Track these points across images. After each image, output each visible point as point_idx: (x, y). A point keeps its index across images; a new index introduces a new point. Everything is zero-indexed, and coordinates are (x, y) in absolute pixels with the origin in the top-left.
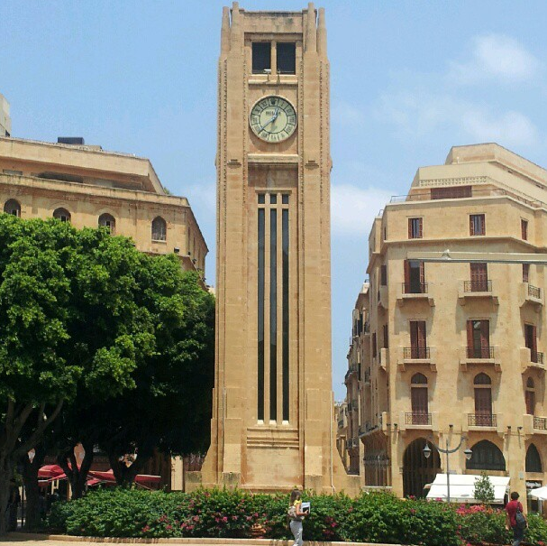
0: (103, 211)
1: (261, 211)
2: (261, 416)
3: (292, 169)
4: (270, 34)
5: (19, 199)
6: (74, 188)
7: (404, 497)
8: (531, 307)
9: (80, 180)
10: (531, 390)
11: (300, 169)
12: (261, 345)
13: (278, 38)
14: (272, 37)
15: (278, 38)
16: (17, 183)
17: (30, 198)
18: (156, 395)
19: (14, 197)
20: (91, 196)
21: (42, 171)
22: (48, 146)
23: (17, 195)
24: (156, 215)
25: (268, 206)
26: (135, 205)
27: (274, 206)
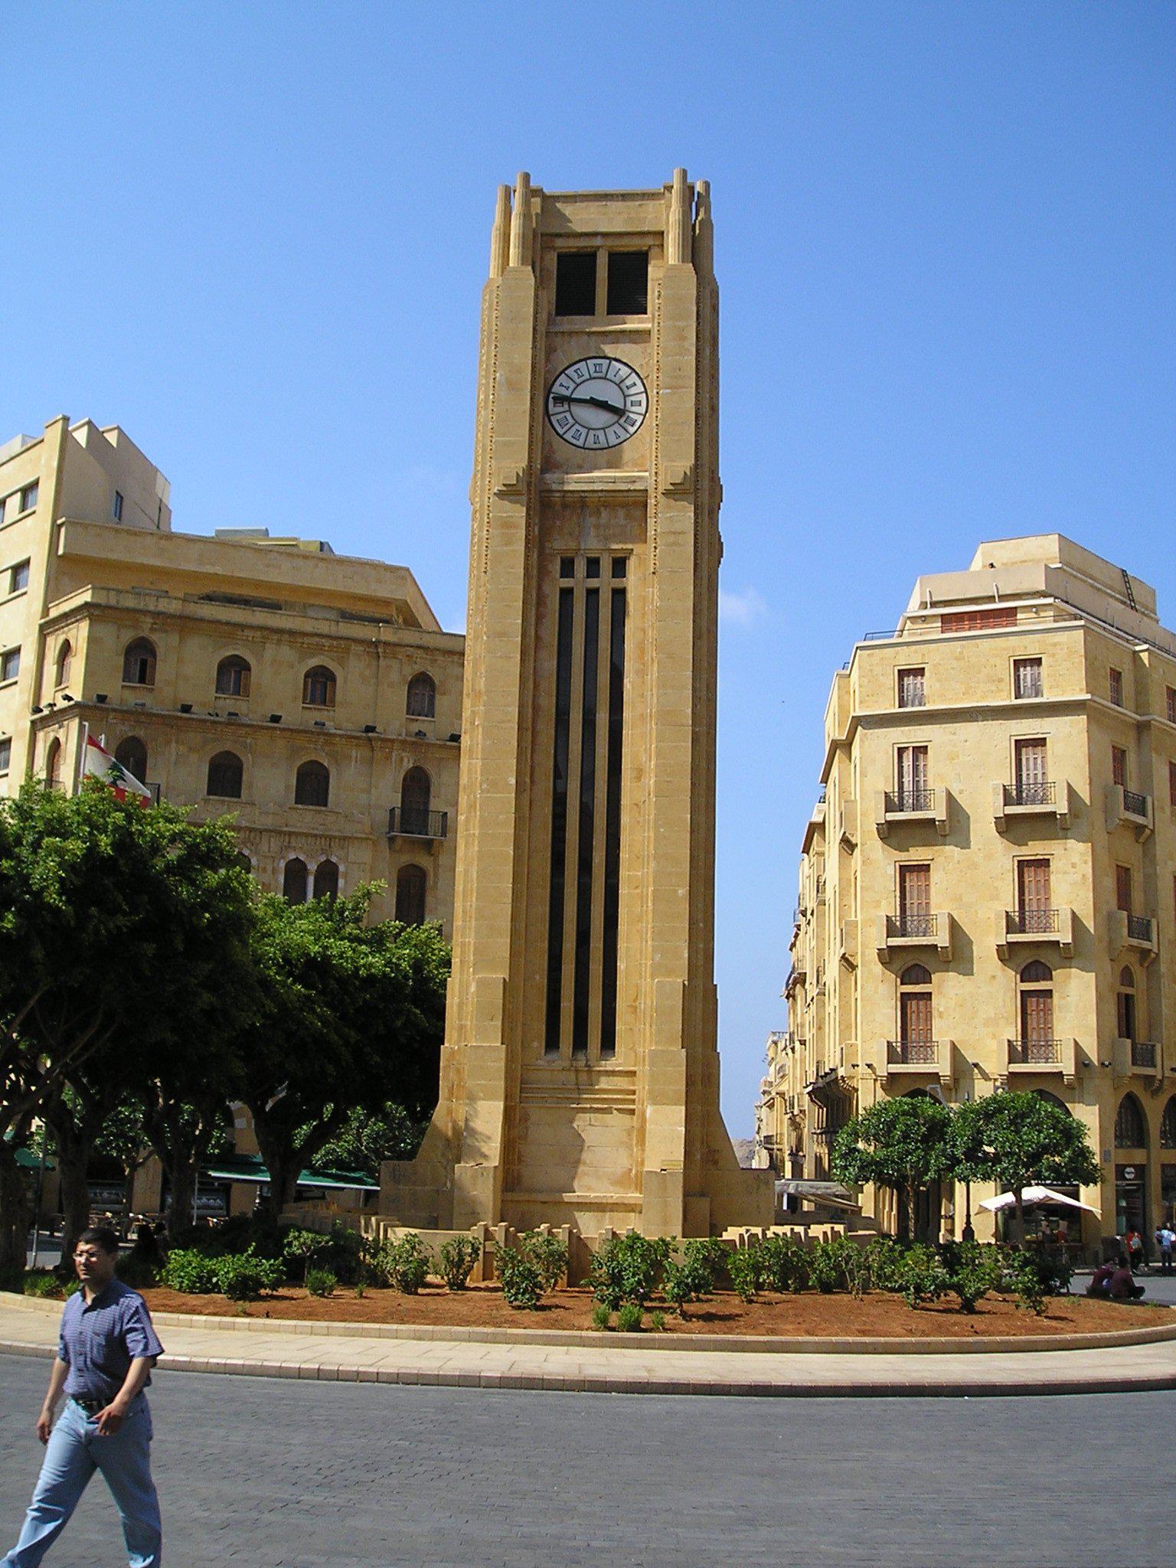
0: (313, 662)
1: (567, 594)
2: (552, 1042)
3: (635, 504)
4: (595, 234)
5: (154, 637)
6: (260, 617)
7: (851, 1293)
8: (825, 780)
9: (274, 606)
10: (1129, 991)
11: (651, 502)
12: (560, 801)
13: (610, 242)
14: (598, 241)
15: (610, 242)
16: (152, 608)
17: (174, 639)
18: (211, 1225)
19: (145, 633)
20: (291, 633)
21: (207, 590)
22: (232, 546)
23: (152, 630)
24: (418, 668)
25: (580, 582)
26: (375, 648)
27: (593, 583)
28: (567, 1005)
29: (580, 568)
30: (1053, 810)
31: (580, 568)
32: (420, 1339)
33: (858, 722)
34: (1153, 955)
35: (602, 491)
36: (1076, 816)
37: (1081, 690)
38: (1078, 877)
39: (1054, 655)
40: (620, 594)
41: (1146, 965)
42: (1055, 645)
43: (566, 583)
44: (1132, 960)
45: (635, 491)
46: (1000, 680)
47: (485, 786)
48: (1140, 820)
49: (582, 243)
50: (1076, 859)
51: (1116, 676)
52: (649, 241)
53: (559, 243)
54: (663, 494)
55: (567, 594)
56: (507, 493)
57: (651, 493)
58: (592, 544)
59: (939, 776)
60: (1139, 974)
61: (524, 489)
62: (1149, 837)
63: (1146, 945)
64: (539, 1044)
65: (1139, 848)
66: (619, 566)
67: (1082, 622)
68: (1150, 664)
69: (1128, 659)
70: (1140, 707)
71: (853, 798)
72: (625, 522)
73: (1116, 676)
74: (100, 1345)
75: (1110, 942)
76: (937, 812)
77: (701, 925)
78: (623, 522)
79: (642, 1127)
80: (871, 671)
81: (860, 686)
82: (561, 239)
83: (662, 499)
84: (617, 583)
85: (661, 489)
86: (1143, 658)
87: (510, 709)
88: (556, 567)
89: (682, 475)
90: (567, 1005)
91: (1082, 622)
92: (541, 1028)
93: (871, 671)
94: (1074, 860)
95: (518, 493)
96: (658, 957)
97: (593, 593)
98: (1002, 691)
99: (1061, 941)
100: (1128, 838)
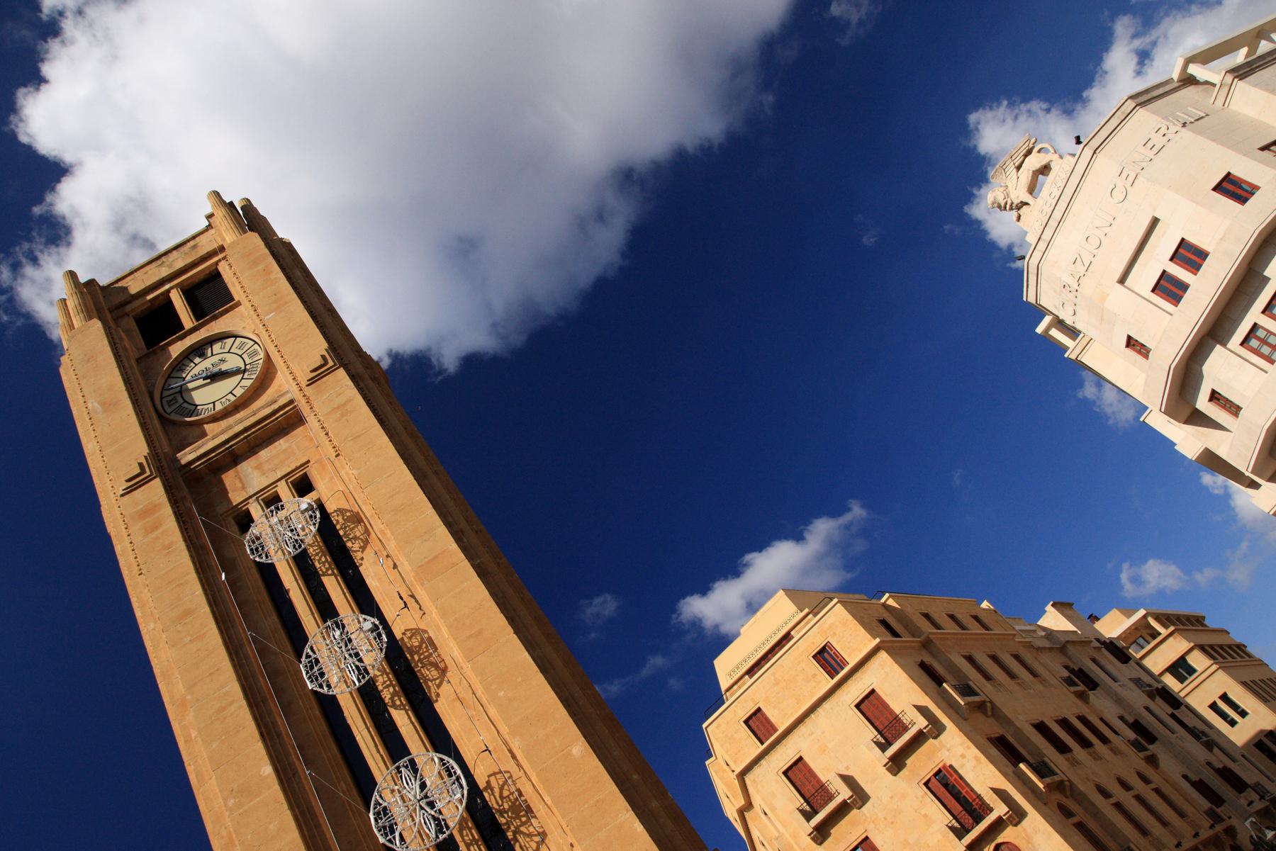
30: (918, 729)
33: (742, 775)
34: (1067, 783)
35: (246, 430)
37: (870, 641)
38: (973, 762)
39: (835, 634)
41: (1068, 793)
42: (830, 626)
44: (1057, 797)
46: (814, 676)
48: (976, 699)
51: (884, 623)
53: (128, 308)
54: (308, 385)
59: (826, 771)
60: (1071, 805)
62: (992, 709)
63: (1056, 778)
65: (991, 720)
68: (899, 605)
69: (882, 610)
70: (914, 631)
71: (777, 834)
72: (287, 445)
73: (884, 623)
74: (1131, 566)
76: (844, 793)
77: (635, 777)
80: (726, 736)
81: (727, 751)
82: (246, 467)
83: (309, 391)
85: (304, 383)
86: (890, 604)
93: (726, 736)
94: (960, 753)
98: (820, 681)
99: (1002, 815)
100: (979, 718)
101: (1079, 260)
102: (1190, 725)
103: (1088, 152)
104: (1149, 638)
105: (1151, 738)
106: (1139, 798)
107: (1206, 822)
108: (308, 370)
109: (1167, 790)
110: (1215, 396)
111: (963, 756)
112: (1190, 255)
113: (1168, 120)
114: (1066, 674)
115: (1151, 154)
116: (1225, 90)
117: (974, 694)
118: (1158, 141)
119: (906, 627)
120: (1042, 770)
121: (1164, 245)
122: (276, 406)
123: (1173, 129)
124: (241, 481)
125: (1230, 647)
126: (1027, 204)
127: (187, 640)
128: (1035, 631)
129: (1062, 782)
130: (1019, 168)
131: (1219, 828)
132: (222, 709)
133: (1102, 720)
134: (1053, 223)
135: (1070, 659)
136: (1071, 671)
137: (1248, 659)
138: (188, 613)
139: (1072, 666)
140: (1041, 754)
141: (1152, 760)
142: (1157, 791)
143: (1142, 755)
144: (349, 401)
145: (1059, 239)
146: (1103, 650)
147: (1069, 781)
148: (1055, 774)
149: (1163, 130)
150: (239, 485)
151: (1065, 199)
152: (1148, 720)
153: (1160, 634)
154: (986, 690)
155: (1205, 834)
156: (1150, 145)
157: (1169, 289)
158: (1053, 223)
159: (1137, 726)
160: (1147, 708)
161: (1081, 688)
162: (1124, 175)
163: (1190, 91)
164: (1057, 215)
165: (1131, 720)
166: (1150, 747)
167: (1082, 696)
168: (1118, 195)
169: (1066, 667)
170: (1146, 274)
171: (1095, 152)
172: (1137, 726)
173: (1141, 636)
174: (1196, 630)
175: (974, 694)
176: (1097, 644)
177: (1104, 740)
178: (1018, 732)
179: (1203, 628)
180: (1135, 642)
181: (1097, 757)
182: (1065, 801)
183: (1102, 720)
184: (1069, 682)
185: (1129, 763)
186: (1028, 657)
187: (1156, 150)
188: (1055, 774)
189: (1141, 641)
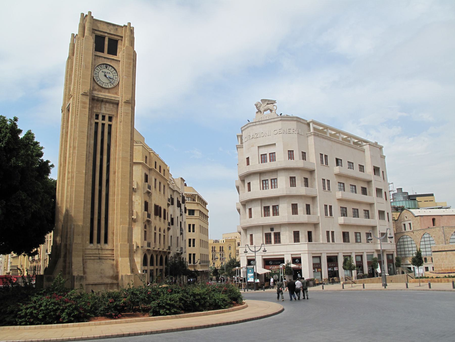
4: (106, 33)
14: (106, 35)
25: (100, 121)
27: (104, 122)
28: (95, 232)
29: (100, 117)
31: (100, 117)
32: (127, 323)
35: (108, 99)
36: (138, 189)
37: (141, 160)
38: (138, 203)
40: (110, 126)
43: (97, 121)
45: (116, 100)
47: (77, 172)
49: (102, 34)
50: (137, 199)
51: (146, 157)
52: (119, 38)
55: (97, 124)
56: (84, 94)
57: (120, 102)
58: (103, 111)
61: (88, 94)
63: (150, 219)
64: (88, 242)
66: (110, 119)
67: (142, 144)
69: (148, 154)
73: (146, 157)
75: (143, 219)
78: (112, 107)
79: (117, 264)
84: (110, 123)
85: (123, 101)
87: (84, 152)
88: (94, 116)
89: (129, 99)
90: (95, 232)
91: (142, 144)
92: (88, 237)
95: (87, 95)
96: (121, 220)
97: (103, 125)
101: (257, 134)
102: (182, 227)
103: (280, 119)
104: (192, 200)
105: (172, 224)
106: (160, 234)
107: (167, 248)
108: (126, 99)
109: (166, 237)
110: (249, 184)
111: (137, 201)
112: (273, 156)
113: (297, 129)
114: (170, 198)
115: (288, 132)
116: (310, 134)
117: (150, 189)
118: (291, 132)
119: (150, 162)
120: (149, 216)
121: (271, 150)
122: (116, 99)
123: (296, 132)
124: (101, 108)
125: (206, 215)
126: (261, 112)
127: (81, 137)
128: (172, 180)
129: (150, 221)
130: (268, 104)
131: (168, 251)
132: (82, 155)
133: (167, 213)
134: (261, 123)
135: (173, 194)
136: (171, 198)
137: (206, 221)
138: (83, 132)
139: (172, 196)
140: (151, 212)
141: (169, 229)
142: (164, 236)
143: (168, 226)
144: (128, 113)
145: (258, 126)
146: (181, 197)
147: (151, 222)
148: (150, 218)
149: (294, 130)
150: (100, 108)
151: (267, 121)
152: (175, 220)
153: (195, 201)
154: (153, 190)
155: (165, 250)
156: (289, 130)
157: (263, 158)
158: (261, 123)
159: (172, 219)
160: (178, 217)
161: (170, 203)
162: (280, 130)
163: (306, 127)
164: (263, 122)
165: (172, 217)
166: (171, 226)
167: (168, 205)
168: (276, 132)
169: (171, 195)
170: (263, 151)
171: (281, 120)
172: (172, 219)
173: (191, 198)
174: (203, 206)
175: (150, 189)
176: (181, 195)
177: (165, 218)
178: (152, 204)
179: (204, 207)
180: (189, 198)
181: (160, 220)
182: (147, 225)
183: (167, 213)
184: (169, 200)
185: (164, 226)
186: (166, 187)
187: (289, 132)
188: (150, 218)
189: (190, 199)
